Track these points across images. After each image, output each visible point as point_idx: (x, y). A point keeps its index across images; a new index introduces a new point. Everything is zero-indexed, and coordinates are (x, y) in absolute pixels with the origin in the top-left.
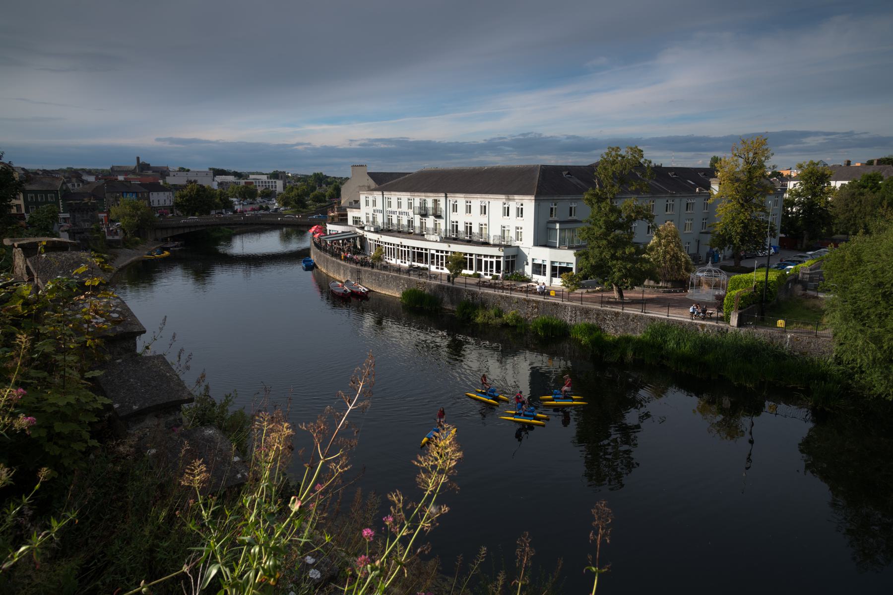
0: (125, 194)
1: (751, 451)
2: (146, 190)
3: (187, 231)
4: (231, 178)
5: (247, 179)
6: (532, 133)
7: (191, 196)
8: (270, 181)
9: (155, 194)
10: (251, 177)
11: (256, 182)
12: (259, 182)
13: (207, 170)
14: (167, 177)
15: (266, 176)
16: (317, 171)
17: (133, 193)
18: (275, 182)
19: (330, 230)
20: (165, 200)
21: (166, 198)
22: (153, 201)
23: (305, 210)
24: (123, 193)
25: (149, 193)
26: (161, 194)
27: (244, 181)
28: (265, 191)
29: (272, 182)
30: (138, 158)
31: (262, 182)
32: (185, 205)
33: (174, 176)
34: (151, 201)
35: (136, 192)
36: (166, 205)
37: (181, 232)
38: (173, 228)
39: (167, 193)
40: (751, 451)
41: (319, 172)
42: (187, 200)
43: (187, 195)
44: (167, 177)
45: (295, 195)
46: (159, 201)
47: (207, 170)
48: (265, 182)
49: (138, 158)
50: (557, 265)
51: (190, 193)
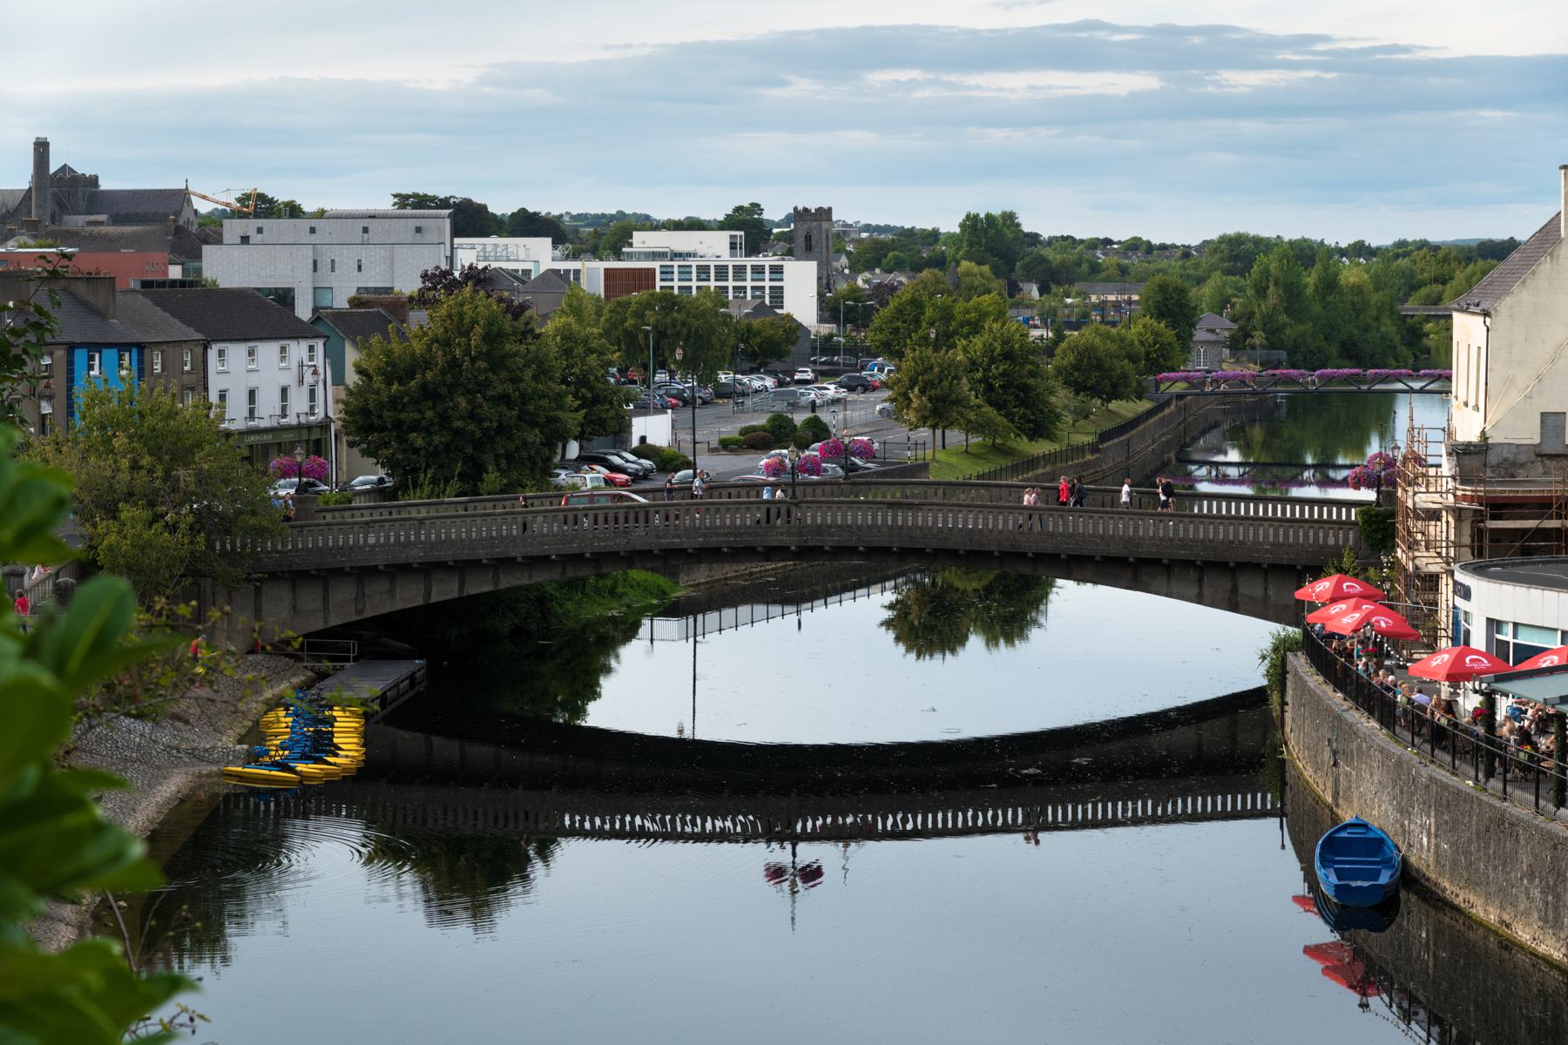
0: (80, 355)
1: (794, 902)
2: (199, 336)
3: (445, 590)
4: (537, 255)
5: (618, 256)
6: (1324, 39)
7: (454, 364)
8: (749, 262)
9: (236, 352)
10: (642, 240)
11: (667, 272)
12: (685, 272)
13: (386, 204)
14: (207, 250)
15: (725, 236)
16: (988, 202)
17: (123, 347)
18: (777, 271)
19: (1494, 625)
20: (284, 391)
21: (289, 379)
22: (222, 397)
23: (1042, 447)
24: (71, 347)
25: (205, 348)
26: (268, 351)
27: (599, 266)
28: (757, 323)
29: (758, 270)
30: (42, 148)
31: (703, 271)
32: (415, 426)
33: (245, 240)
34: (213, 398)
35: (141, 347)
36: (291, 420)
37: (408, 596)
38: (364, 573)
39: (298, 350)
40: (794, 902)
41: (996, 212)
42: (428, 393)
43: (427, 363)
44: (207, 250)
45: (989, 349)
46: (252, 394)
47: (386, 204)
48: (721, 272)
49: (42, 148)
50: (1507, 636)
51: (446, 344)
